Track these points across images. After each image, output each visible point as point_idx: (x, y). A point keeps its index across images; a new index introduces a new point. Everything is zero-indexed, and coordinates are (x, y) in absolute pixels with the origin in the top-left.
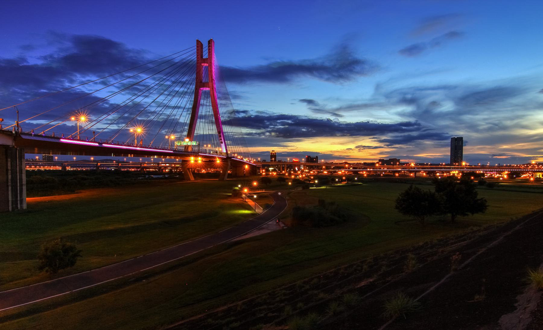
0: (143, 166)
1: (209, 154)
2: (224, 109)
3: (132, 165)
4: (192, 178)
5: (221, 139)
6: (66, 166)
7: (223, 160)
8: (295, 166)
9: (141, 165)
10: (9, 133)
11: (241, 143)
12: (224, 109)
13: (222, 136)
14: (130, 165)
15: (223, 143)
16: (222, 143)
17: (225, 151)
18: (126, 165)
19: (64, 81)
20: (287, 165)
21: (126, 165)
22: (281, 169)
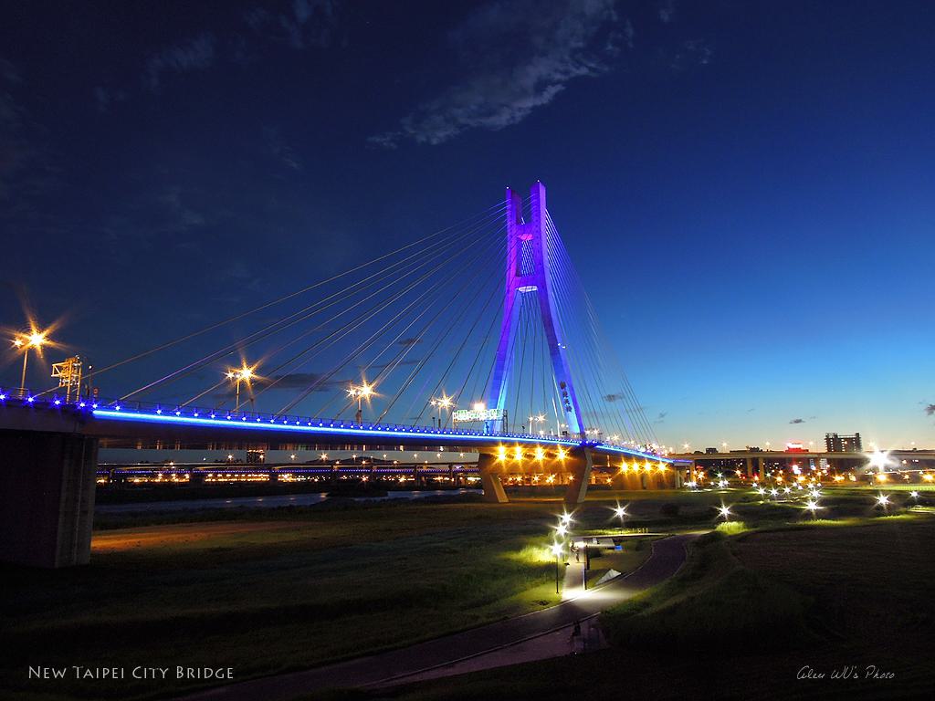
0: (419, 470)
1: (491, 435)
2: (636, 417)
3: (398, 468)
4: (503, 498)
5: (567, 401)
6: (279, 473)
7: (574, 452)
8: (792, 461)
9: (415, 468)
10: (687, 457)
11: (628, 409)
12: (636, 417)
13: (569, 394)
14: (394, 468)
15: (573, 410)
16: (569, 409)
17: (577, 429)
18: (387, 468)
19: (496, 397)
20: (765, 460)
21: (387, 468)
22: (750, 470)
